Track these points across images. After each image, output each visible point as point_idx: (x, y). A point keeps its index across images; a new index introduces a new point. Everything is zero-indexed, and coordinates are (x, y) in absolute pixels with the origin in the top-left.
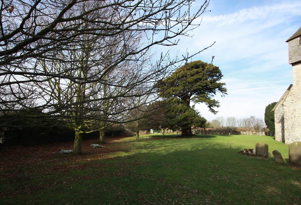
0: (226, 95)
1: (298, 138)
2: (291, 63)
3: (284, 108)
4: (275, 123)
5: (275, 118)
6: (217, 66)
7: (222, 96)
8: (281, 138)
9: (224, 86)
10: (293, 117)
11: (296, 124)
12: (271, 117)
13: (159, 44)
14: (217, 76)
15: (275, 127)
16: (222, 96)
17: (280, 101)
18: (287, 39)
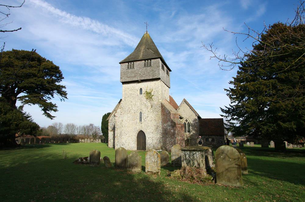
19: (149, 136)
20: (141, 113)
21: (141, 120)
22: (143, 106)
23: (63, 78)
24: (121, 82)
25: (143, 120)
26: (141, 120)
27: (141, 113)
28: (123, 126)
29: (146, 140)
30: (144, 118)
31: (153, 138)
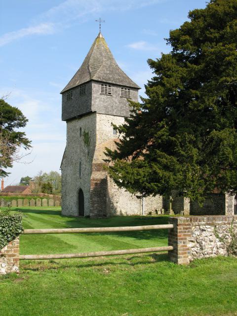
22: (82, 154)
23: (27, 120)
27: (80, 163)
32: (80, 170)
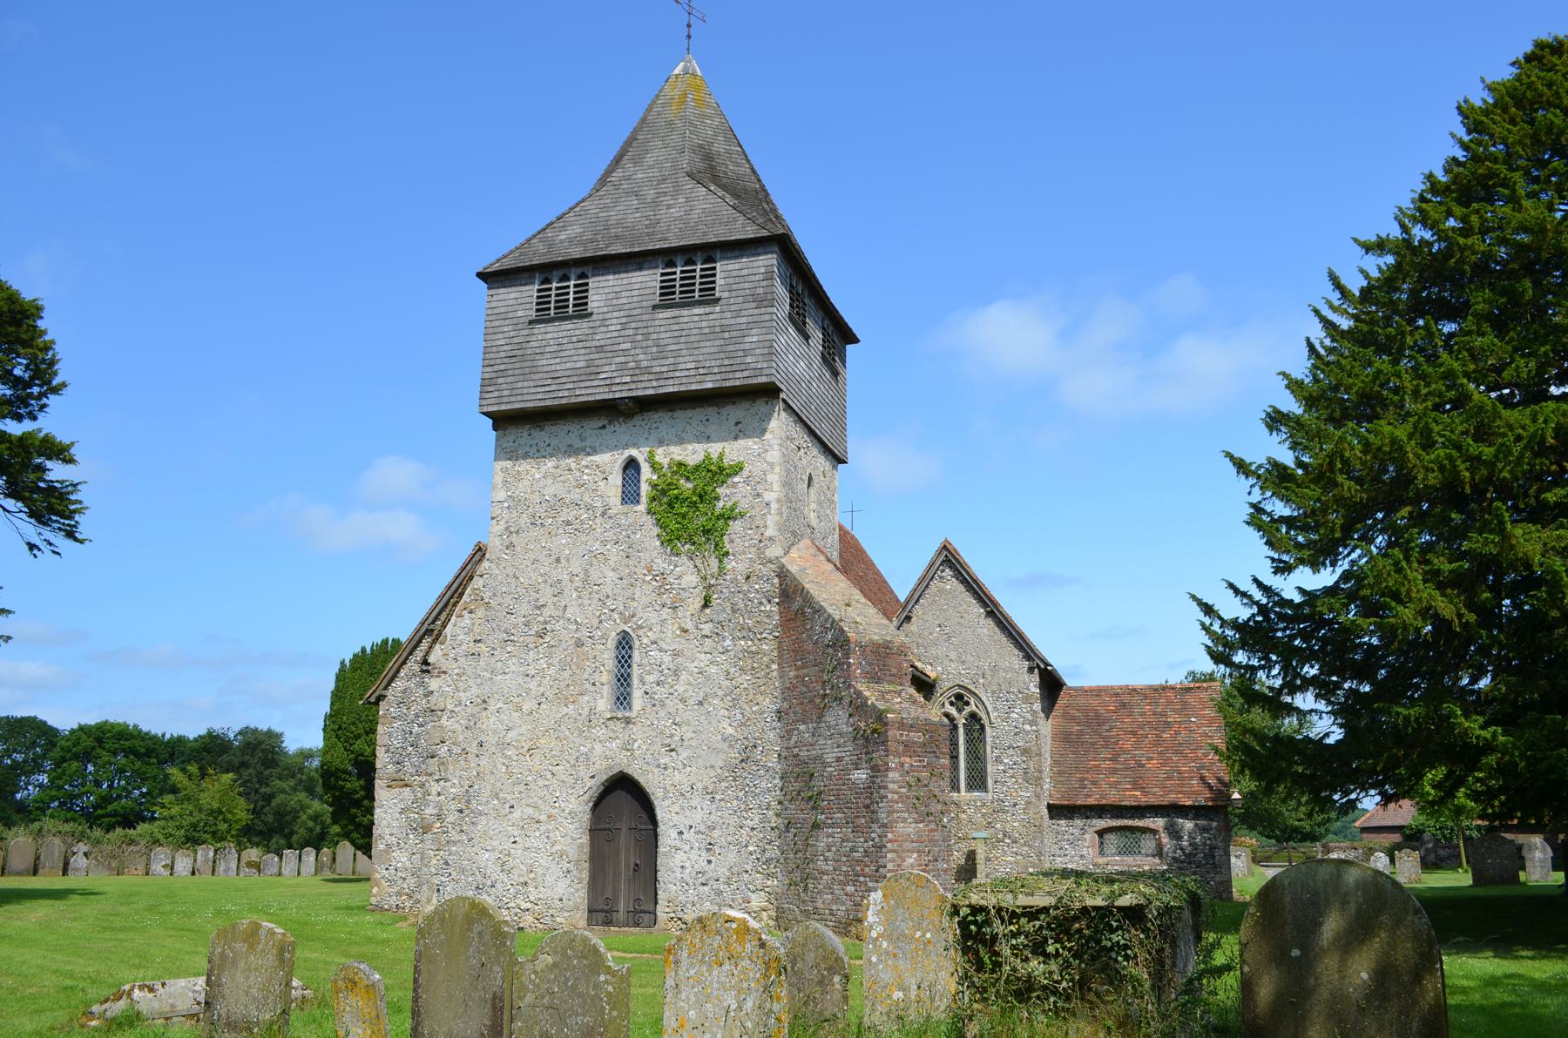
0: (60, 541)
1: (489, 883)
2: (490, 409)
3: (434, 684)
4: (378, 783)
5: (380, 752)
6: (27, 295)
7: (32, 547)
8: (646, 909)
9: (57, 472)
10: (473, 749)
11: (486, 792)
12: (359, 745)
13: (1523, 957)
14: (18, 380)
15: (377, 811)
16: (32, 547)
17: (416, 642)
18: (489, 258)
19: (682, 821)
20: (625, 644)
21: (623, 699)
24: (487, 414)
25: (637, 694)
26: (623, 699)
27: (625, 644)
28: (491, 740)
29: (661, 849)
30: (650, 678)
31: (716, 833)
32: (623, 680)
